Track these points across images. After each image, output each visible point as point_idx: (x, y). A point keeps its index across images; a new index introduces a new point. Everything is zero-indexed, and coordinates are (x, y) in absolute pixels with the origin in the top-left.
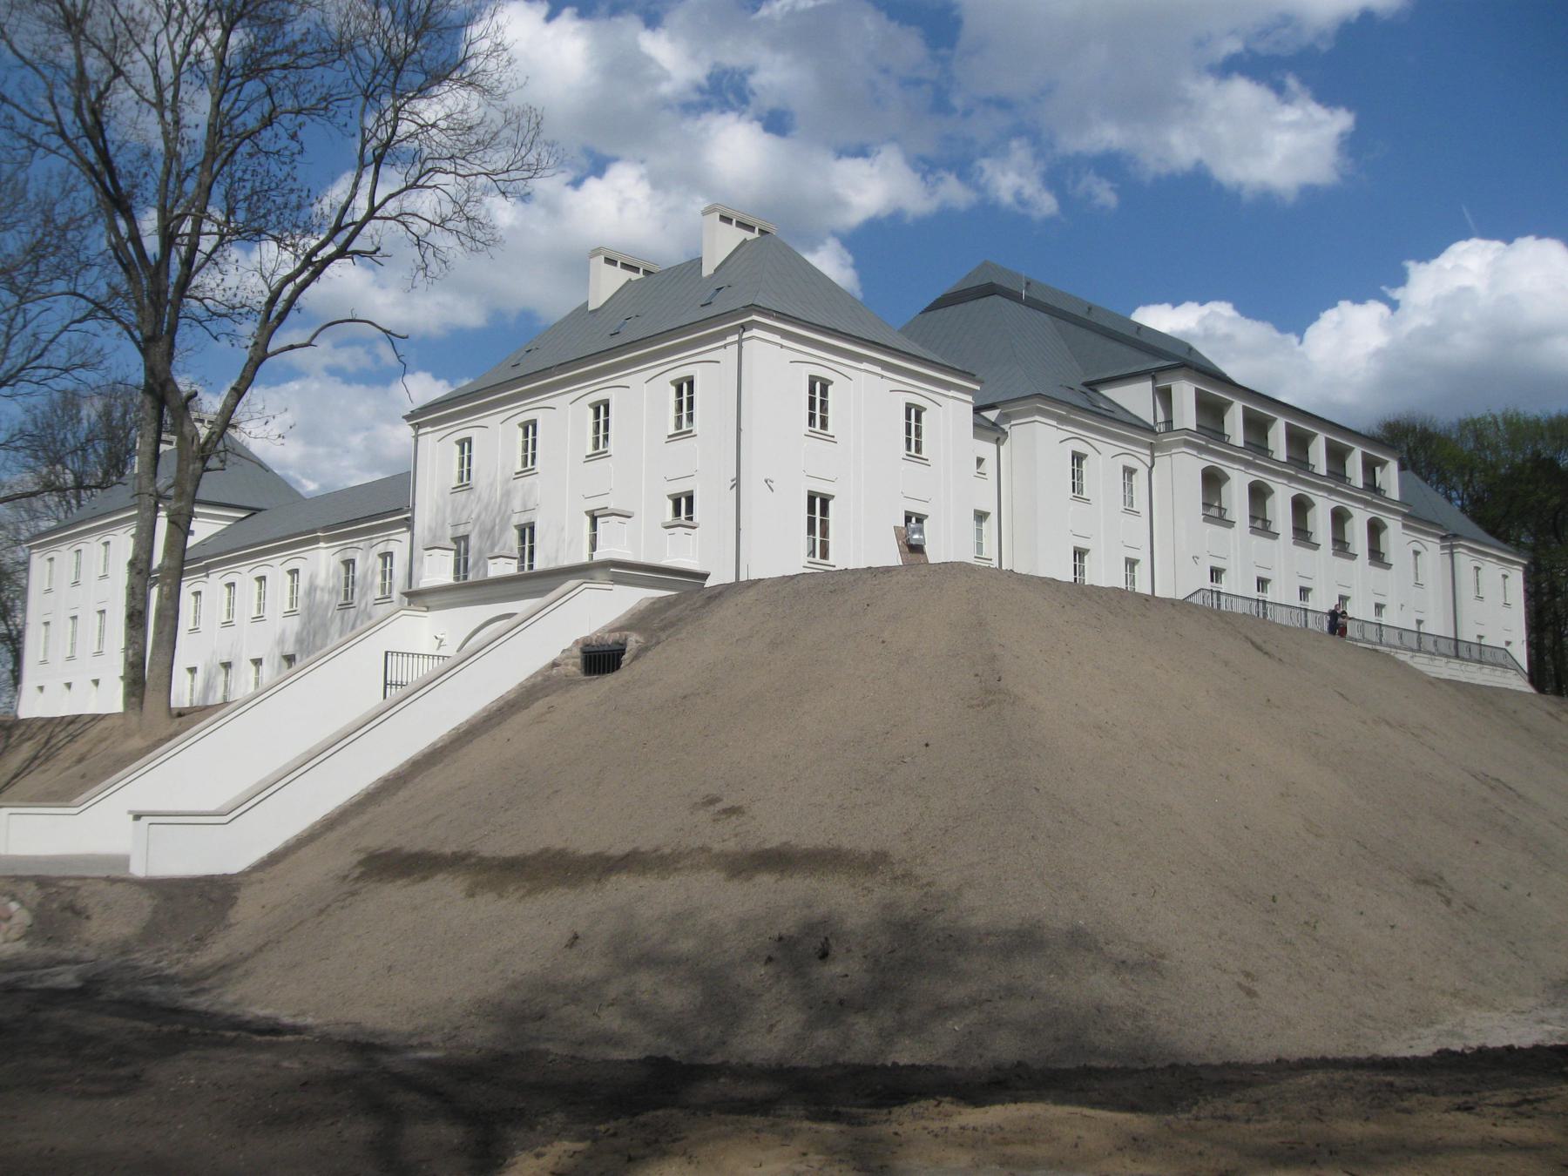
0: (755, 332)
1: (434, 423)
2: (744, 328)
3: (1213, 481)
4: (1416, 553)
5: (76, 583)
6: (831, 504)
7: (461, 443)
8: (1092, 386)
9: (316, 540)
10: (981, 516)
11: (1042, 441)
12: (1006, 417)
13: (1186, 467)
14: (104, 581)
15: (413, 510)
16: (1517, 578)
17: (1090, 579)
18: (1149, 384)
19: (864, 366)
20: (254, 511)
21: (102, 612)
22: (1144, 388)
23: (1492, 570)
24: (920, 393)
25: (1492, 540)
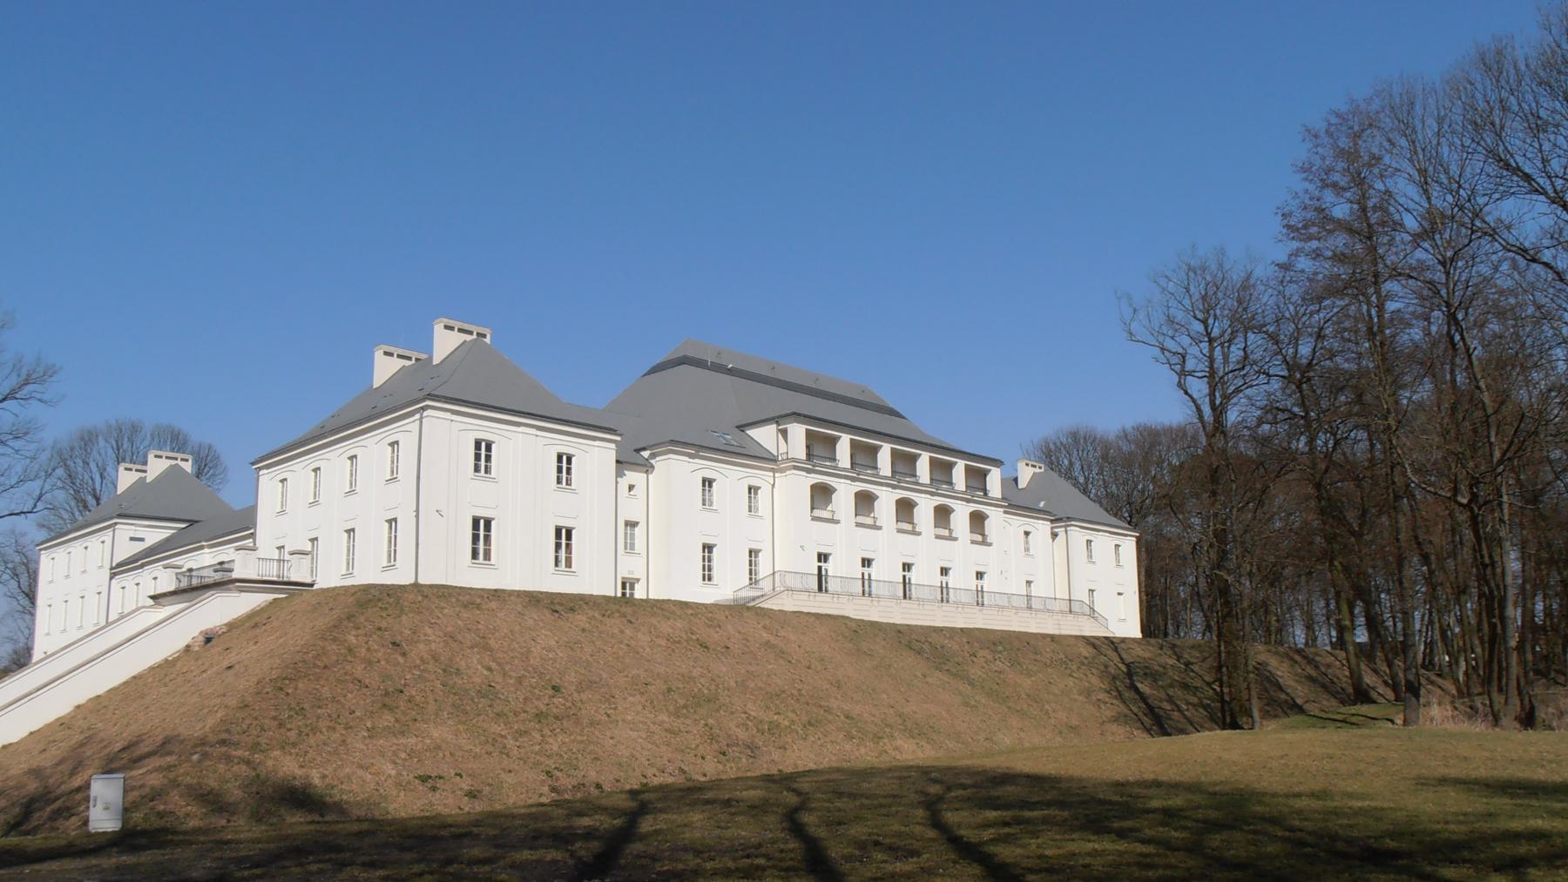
0: (428, 412)
1: (268, 467)
2: (423, 409)
3: (821, 494)
4: (1027, 534)
5: (315, 503)
6: (493, 523)
7: (392, 444)
8: (742, 428)
9: (202, 548)
10: (631, 525)
11: (676, 473)
12: (653, 456)
13: (798, 485)
14: (392, 486)
15: (255, 526)
16: (1129, 546)
17: (421, 581)
18: (774, 426)
19: (521, 429)
20: (192, 522)
21: (350, 531)
22: (772, 429)
23: (1104, 542)
24: (566, 444)
25: (1114, 520)
